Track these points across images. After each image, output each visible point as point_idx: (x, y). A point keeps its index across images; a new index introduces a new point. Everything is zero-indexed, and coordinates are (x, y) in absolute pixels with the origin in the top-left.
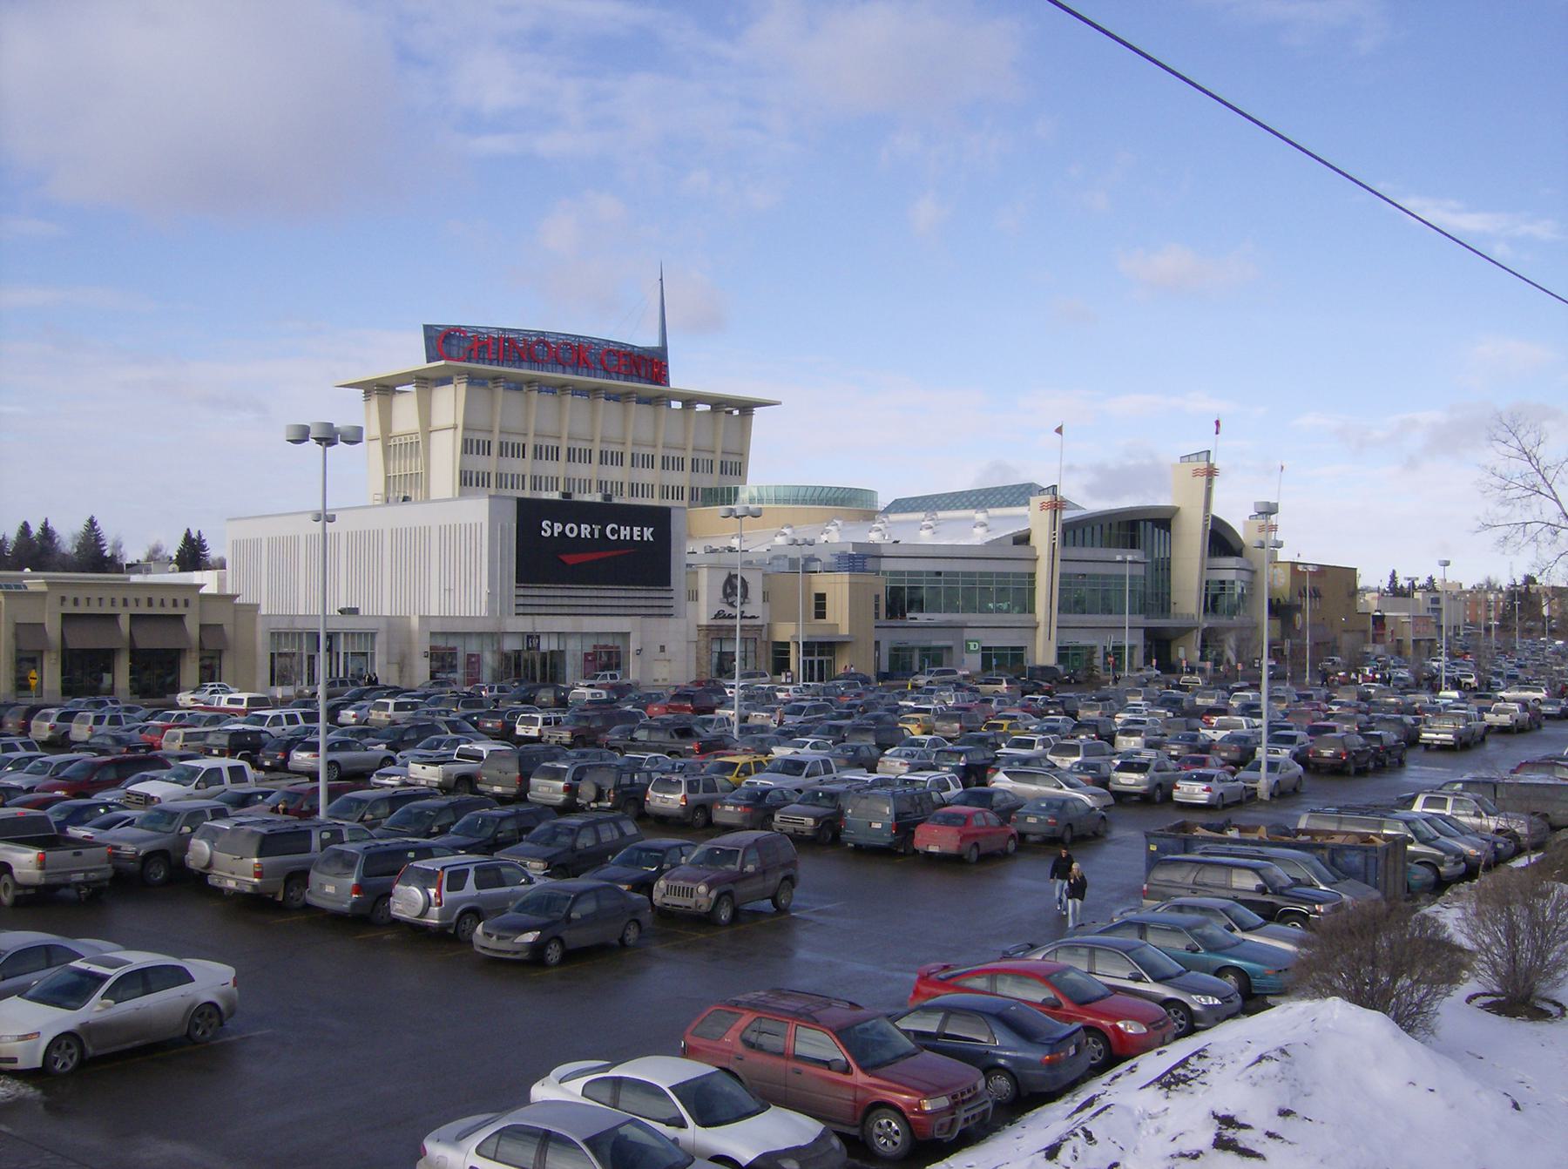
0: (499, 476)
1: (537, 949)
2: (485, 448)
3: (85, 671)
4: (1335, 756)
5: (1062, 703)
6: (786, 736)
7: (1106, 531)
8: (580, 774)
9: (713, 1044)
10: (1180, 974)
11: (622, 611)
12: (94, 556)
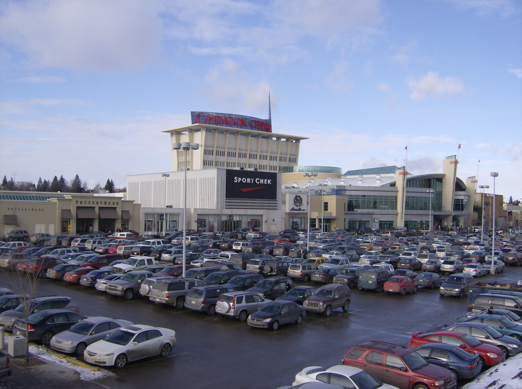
0: (216, 162)
1: (271, 324)
2: (211, 153)
3: (84, 226)
4: (513, 260)
5: (413, 240)
6: (326, 251)
7: (421, 182)
8: (264, 263)
9: (356, 361)
10: (501, 337)
11: (261, 207)
12: (78, 187)
